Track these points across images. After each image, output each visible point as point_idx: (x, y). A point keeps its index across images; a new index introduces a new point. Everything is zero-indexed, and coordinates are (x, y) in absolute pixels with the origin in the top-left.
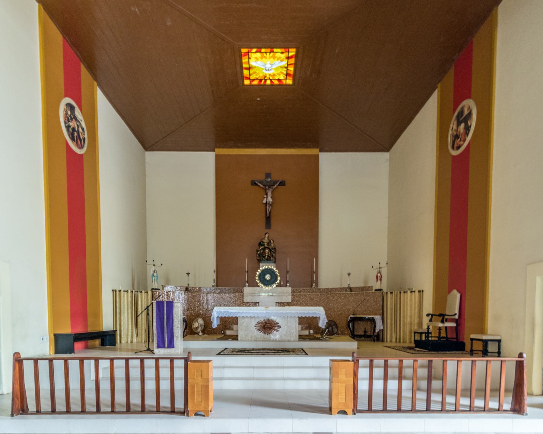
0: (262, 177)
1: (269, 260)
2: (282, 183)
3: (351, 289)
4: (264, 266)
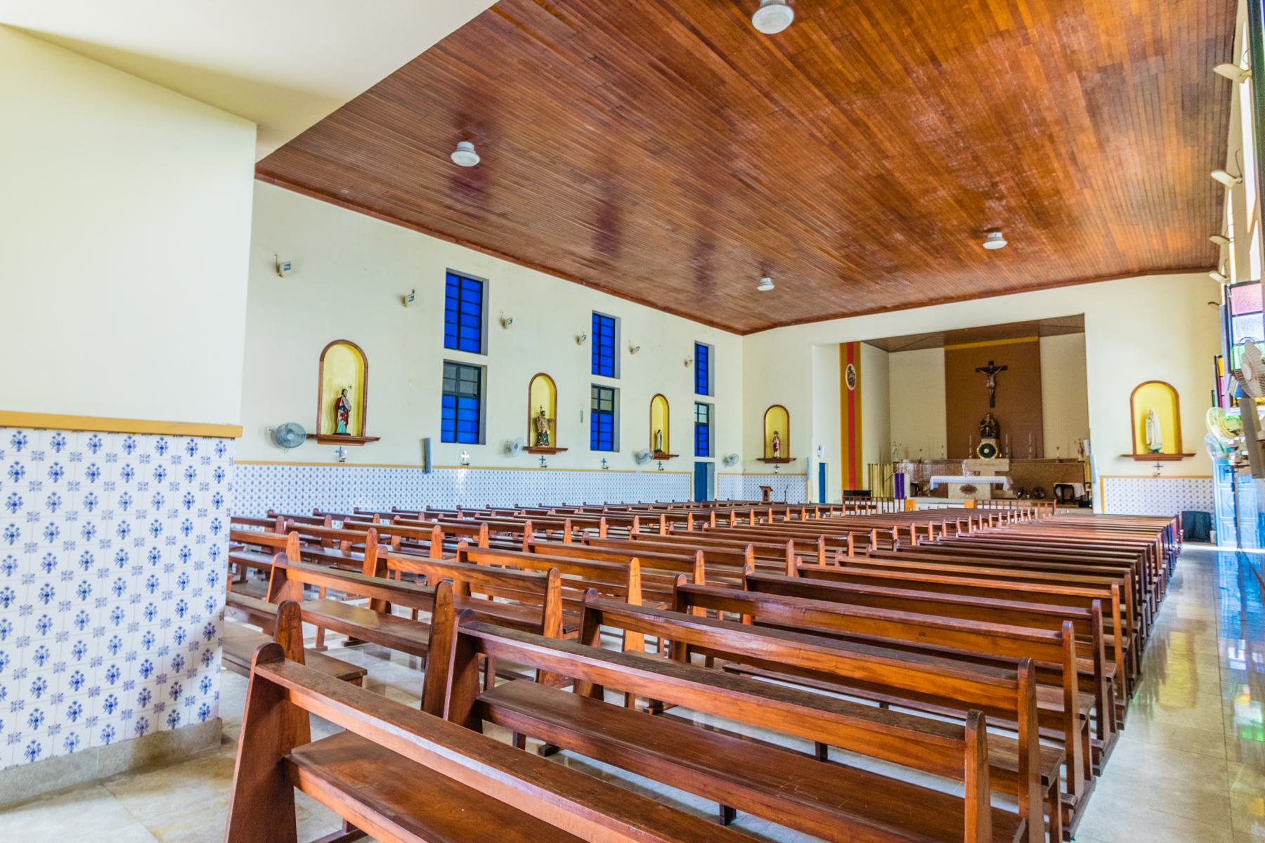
0: (985, 365)
1: (989, 436)
2: (1005, 368)
3: (1061, 461)
4: (984, 442)
